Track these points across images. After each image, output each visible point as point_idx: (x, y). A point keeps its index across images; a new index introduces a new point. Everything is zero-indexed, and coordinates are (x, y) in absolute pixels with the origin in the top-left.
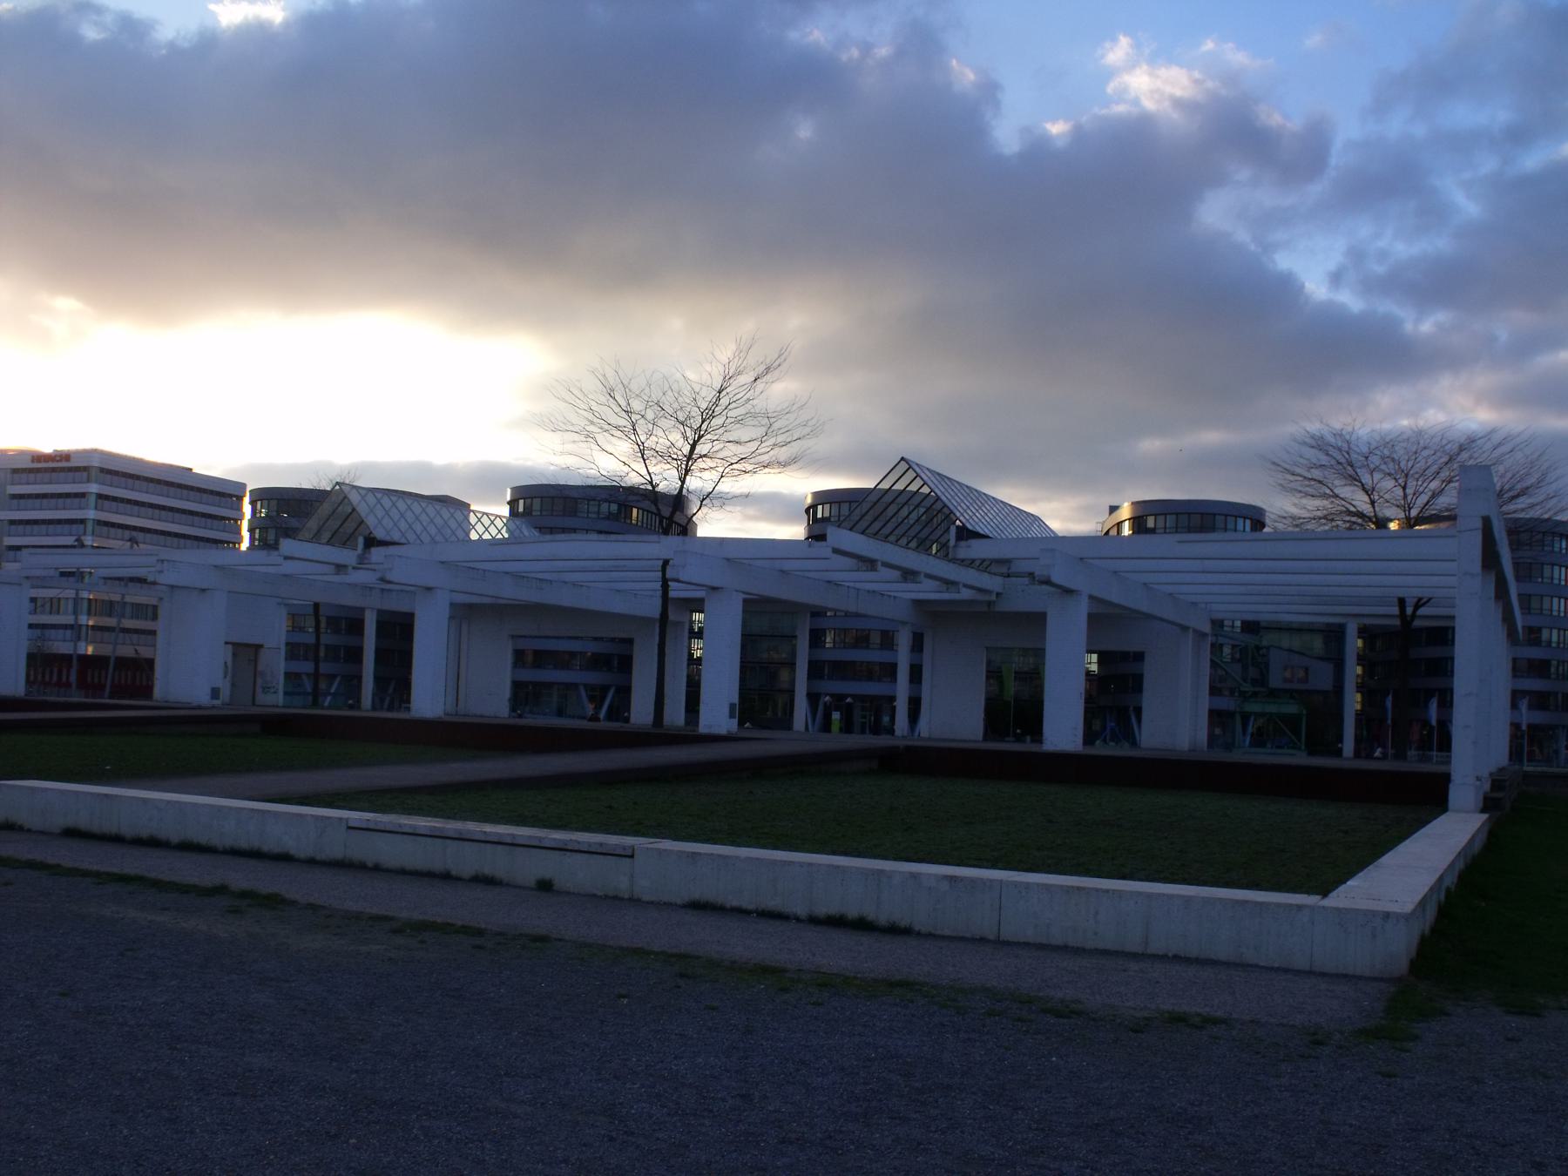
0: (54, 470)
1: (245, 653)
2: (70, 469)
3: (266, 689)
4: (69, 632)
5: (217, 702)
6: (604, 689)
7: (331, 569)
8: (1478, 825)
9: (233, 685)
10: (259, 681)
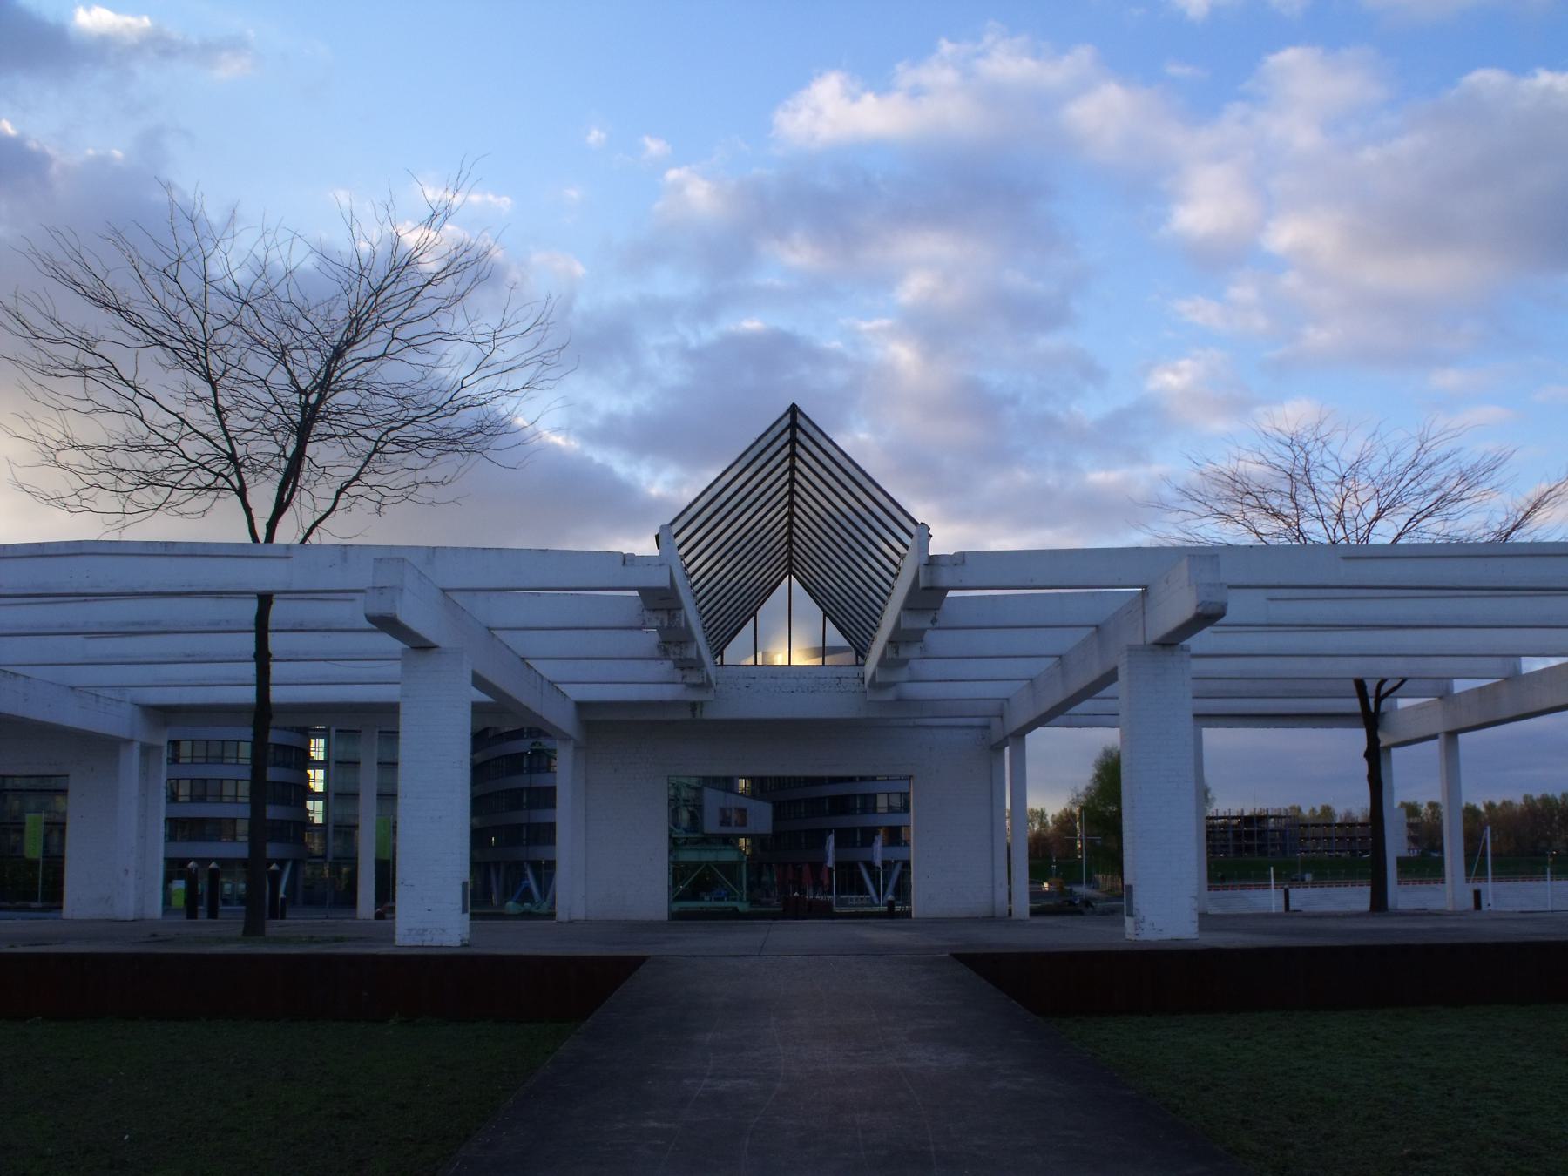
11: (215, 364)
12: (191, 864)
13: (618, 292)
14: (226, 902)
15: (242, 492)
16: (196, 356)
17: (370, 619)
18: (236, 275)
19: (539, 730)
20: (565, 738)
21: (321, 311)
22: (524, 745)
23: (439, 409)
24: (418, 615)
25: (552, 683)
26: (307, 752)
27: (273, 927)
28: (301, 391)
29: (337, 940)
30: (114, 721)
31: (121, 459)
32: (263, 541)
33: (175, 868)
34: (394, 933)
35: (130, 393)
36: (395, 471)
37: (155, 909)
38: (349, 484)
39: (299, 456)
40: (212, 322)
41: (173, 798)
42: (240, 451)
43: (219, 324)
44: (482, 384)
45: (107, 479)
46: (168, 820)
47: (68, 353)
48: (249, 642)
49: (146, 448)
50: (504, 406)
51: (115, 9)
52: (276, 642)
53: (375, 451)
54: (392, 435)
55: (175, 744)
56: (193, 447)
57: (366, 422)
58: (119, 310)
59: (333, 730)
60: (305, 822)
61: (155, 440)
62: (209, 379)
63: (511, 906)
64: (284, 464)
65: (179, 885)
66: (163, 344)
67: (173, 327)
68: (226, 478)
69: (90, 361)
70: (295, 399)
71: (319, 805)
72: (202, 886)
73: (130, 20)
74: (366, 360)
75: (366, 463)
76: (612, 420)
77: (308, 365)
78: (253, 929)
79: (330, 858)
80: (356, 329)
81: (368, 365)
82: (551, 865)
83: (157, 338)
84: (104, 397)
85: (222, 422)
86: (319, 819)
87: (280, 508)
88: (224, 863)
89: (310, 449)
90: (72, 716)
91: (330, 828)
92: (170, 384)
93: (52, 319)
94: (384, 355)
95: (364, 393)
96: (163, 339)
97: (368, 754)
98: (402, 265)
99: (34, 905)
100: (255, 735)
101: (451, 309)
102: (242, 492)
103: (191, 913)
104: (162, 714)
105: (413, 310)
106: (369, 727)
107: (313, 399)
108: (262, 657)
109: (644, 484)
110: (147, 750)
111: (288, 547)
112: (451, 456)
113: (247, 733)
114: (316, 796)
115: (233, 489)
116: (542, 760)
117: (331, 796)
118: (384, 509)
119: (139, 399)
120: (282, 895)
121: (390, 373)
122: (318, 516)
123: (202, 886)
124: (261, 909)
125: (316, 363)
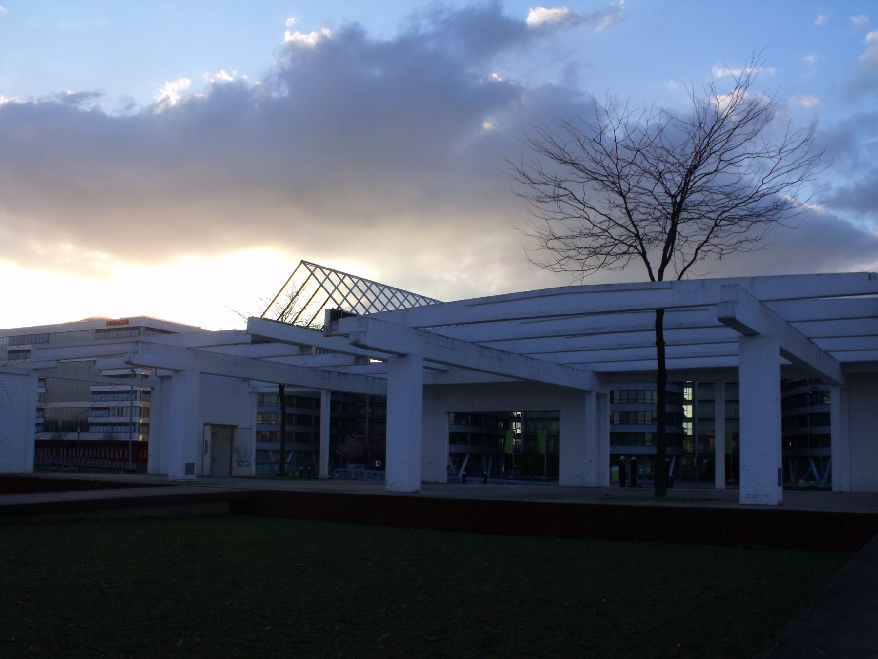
0: (119, 329)
1: (222, 434)
2: (128, 329)
3: (240, 463)
4: (128, 427)
5: (192, 477)
6: (462, 456)
7: (295, 349)
8: (591, 480)
9: (213, 460)
10: (235, 456)
11: (624, 186)
12: (622, 458)
13: (834, 119)
14: (640, 478)
15: (644, 255)
16: (614, 183)
17: (721, 320)
18: (632, 136)
19: (818, 379)
20: (835, 384)
21: (678, 151)
22: (807, 389)
23: (750, 198)
24: (747, 316)
25: (826, 352)
26: (682, 395)
27: (670, 493)
28: (670, 195)
29: (706, 500)
30: (581, 381)
31: (579, 243)
32: (657, 281)
33: (614, 459)
34: (739, 496)
35: (582, 207)
36: (728, 235)
37: (606, 483)
38: (702, 245)
39: (673, 231)
40: (621, 164)
41: (612, 422)
42: (641, 232)
43: (624, 165)
44: (774, 181)
45: (573, 253)
46: (611, 434)
47: (549, 190)
48: (652, 336)
49: (592, 235)
50: (785, 195)
51: (548, 7)
52: (667, 335)
53: (716, 225)
54: (724, 215)
55: (612, 393)
56: (616, 232)
57: (708, 209)
58: (573, 164)
59: (696, 383)
60: (682, 434)
61: (596, 230)
62: (621, 194)
63: (802, 483)
64: (665, 237)
65: (616, 469)
66: (596, 179)
67: (601, 169)
68: (635, 247)
69: (561, 192)
70: (669, 200)
71: (690, 425)
72: (628, 469)
73: (554, 11)
74: (706, 174)
75: (711, 232)
76: (842, 191)
77: (675, 180)
78: (660, 494)
79: (696, 454)
80: (700, 157)
81: (708, 176)
82: (827, 458)
83: (592, 176)
84: (568, 209)
85: (630, 216)
86: (690, 433)
87: (665, 261)
88: (640, 457)
89: (679, 228)
90: (562, 379)
91: (697, 437)
92: (602, 200)
93: (540, 173)
94: (716, 171)
95: (706, 193)
96: (596, 176)
97: (720, 397)
98: (720, 120)
99: (542, 478)
100: (658, 387)
101: (753, 140)
102: (644, 255)
103: (622, 484)
104: (605, 377)
105: (730, 143)
106: (720, 383)
107: (678, 199)
108: (660, 344)
109: (871, 230)
110: (599, 396)
111: (671, 282)
112: (758, 224)
113: (654, 386)
114: (688, 420)
115: (639, 253)
116: (818, 397)
117: (696, 420)
118: (723, 257)
119: (586, 209)
120: (671, 475)
121: (719, 180)
122: (686, 264)
123: (628, 469)
124: (662, 483)
125: (678, 179)
